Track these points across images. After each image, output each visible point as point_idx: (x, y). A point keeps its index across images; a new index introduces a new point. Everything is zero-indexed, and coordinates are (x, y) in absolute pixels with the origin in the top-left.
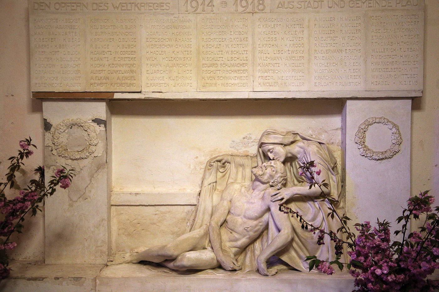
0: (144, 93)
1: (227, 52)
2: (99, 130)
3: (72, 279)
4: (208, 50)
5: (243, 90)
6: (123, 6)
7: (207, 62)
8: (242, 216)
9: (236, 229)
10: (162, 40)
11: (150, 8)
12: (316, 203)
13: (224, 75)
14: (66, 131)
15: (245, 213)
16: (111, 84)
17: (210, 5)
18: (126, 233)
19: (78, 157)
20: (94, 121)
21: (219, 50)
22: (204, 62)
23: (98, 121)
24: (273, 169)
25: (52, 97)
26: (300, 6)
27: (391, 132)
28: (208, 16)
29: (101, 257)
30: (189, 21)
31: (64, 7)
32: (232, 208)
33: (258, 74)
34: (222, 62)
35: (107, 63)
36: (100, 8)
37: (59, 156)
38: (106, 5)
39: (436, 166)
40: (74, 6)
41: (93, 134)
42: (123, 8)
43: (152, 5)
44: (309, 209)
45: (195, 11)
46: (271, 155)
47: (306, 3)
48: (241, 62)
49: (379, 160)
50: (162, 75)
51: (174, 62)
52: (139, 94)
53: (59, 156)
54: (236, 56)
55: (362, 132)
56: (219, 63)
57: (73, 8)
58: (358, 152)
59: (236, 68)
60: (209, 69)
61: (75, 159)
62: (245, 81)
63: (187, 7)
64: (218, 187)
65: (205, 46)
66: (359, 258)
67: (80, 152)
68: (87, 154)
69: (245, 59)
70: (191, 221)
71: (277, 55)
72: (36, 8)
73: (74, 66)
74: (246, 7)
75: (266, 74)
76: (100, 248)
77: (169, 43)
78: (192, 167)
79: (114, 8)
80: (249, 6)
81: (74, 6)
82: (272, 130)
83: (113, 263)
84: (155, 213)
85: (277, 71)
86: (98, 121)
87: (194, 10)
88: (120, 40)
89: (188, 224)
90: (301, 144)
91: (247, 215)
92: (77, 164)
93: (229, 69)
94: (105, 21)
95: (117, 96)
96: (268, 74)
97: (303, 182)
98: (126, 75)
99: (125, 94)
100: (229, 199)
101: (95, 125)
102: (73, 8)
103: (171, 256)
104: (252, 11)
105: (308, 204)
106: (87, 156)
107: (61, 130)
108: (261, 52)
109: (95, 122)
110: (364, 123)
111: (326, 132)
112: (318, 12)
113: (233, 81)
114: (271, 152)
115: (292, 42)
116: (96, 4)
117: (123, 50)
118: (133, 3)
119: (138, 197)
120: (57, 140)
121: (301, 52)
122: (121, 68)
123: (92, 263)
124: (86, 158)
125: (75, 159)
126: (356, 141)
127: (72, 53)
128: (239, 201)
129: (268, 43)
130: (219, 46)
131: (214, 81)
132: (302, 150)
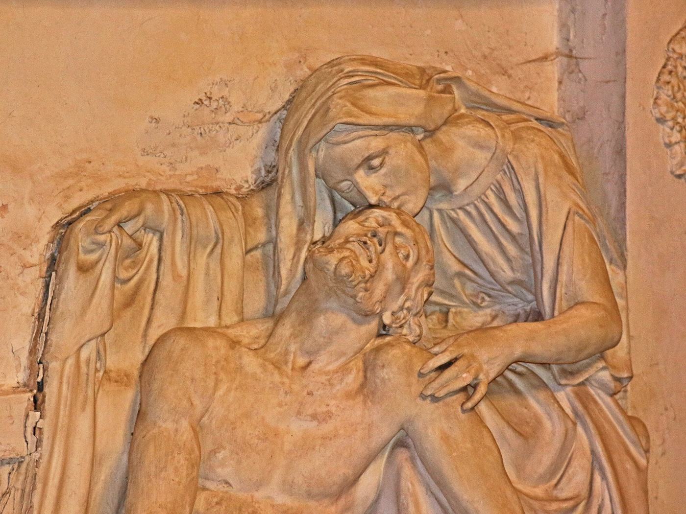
82: (29, 499)
111: (505, 73)
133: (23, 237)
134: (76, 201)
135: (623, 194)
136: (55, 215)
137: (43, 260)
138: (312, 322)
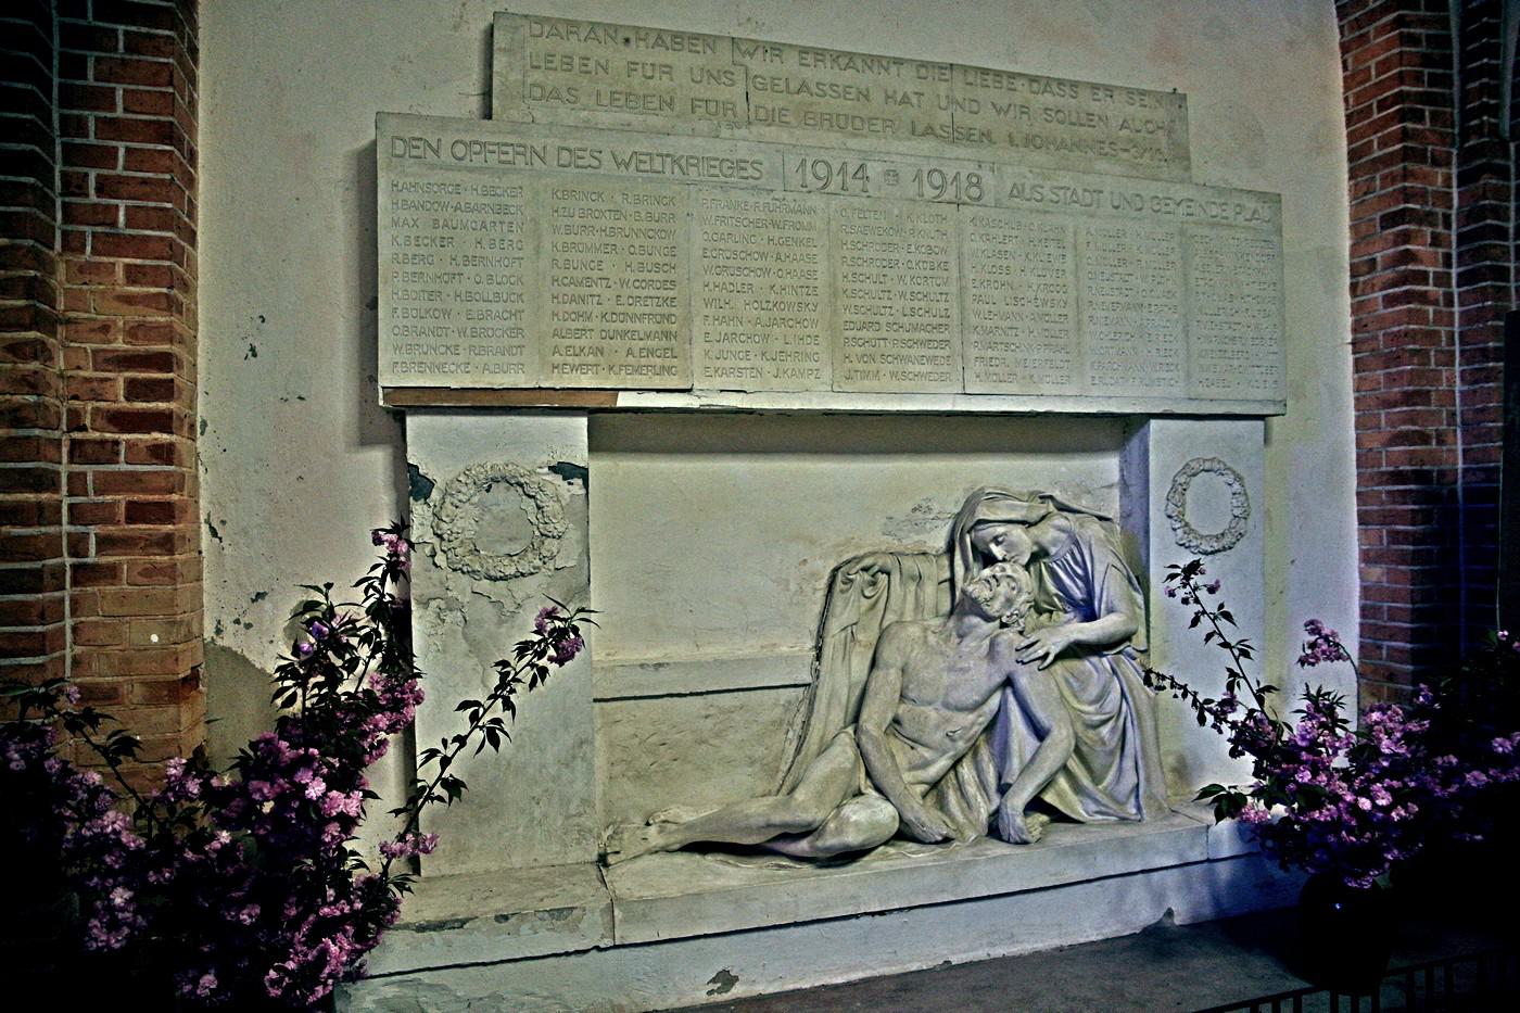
0: (698, 393)
1: (902, 295)
2: (567, 495)
3: (546, 915)
4: (858, 286)
5: (942, 391)
6: (641, 162)
7: (854, 318)
8: (938, 705)
9: (925, 738)
10: (743, 255)
11: (712, 171)
12: (1104, 659)
13: (894, 351)
14: (475, 499)
15: (946, 694)
16: (611, 368)
17: (860, 174)
18: (630, 774)
19: (511, 571)
20: (553, 469)
21: (882, 287)
22: (848, 316)
23: (566, 471)
24: (1013, 584)
25: (443, 401)
26: (1055, 198)
27: (1230, 490)
28: (856, 202)
29: (579, 844)
30: (811, 211)
31: (479, 153)
32: (911, 686)
33: (973, 352)
34: (891, 319)
35: (597, 310)
36: (580, 162)
37: (455, 570)
38: (596, 154)
39: (1293, 562)
40: (507, 153)
41: (551, 507)
42: (642, 167)
43: (717, 163)
44: (1091, 673)
45: (823, 188)
46: (997, 551)
47: (1069, 193)
48: (936, 321)
49: (1212, 553)
50: (746, 347)
51: (776, 313)
52: (686, 395)
53: (455, 570)
54: (922, 304)
55: (1178, 490)
56: (883, 320)
57: (503, 157)
58: (1171, 538)
59: (923, 335)
60: (860, 334)
61: (501, 579)
62: (945, 368)
63: (804, 175)
64: (860, 637)
65: (850, 278)
66: (1319, 778)
67: (515, 558)
68: (538, 563)
69: (943, 313)
70: (798, 728)
71: (1011, 308)
72: (398, 152)
73: (506, 315)
74: (942, 188)
75: (990, 353)
76: (576, 820)
77: (760, 264)
78: (793, 587)
79: (618, 165)
80: (949, 187)
81: (507, 153)
82: (995, 488)
83: (622, 856)
84: (704, 713)
85: (1013, 347)
86: (566, 471)
87: (821, 184)
88: (632, 250)
89: (791, 734)
90: (1059, 521)
91: (951, 700)
92: (505, 592)
93: (907, 336)
94: (594, 197)
95: (624, 400)
96: (995, 354)
97: (1051, 612)
98: (651, 343)
99: (646, 395)
100: (899, 664)
101: (558, 479)
102: (503, 157)
103: (809, 825)
104: (954, 200)
105: (1087, 663)
106: (534, 568)
107: (461, 497)
108: (978, 299)
109: (556, 473)
110: (1182, 472)
111: (1089, 492)
112: (1092, 216)
113: (917, 368)
114: (998, 544)
115: (1042, 281)
116: (570, 151)
117: (641, 276)
118: (668, 156)
119: (663, 673)
120: (450, 526)
121: (1062, 304)
122: (637, 326)
123: (555, 862)
124: (532, 574)
125: (501, 579)
126: (1169, 513)
127: (499, 280)
128: (926, 667)
129: (992, 278)
130: (882, 279)
131: (873, 367)
132: (1063, 536)
133: (815, 575)
134: (846, 557)
135: (1148, 555)
136: (833, 565)
137: (561, 74)
138: (361, 777)
